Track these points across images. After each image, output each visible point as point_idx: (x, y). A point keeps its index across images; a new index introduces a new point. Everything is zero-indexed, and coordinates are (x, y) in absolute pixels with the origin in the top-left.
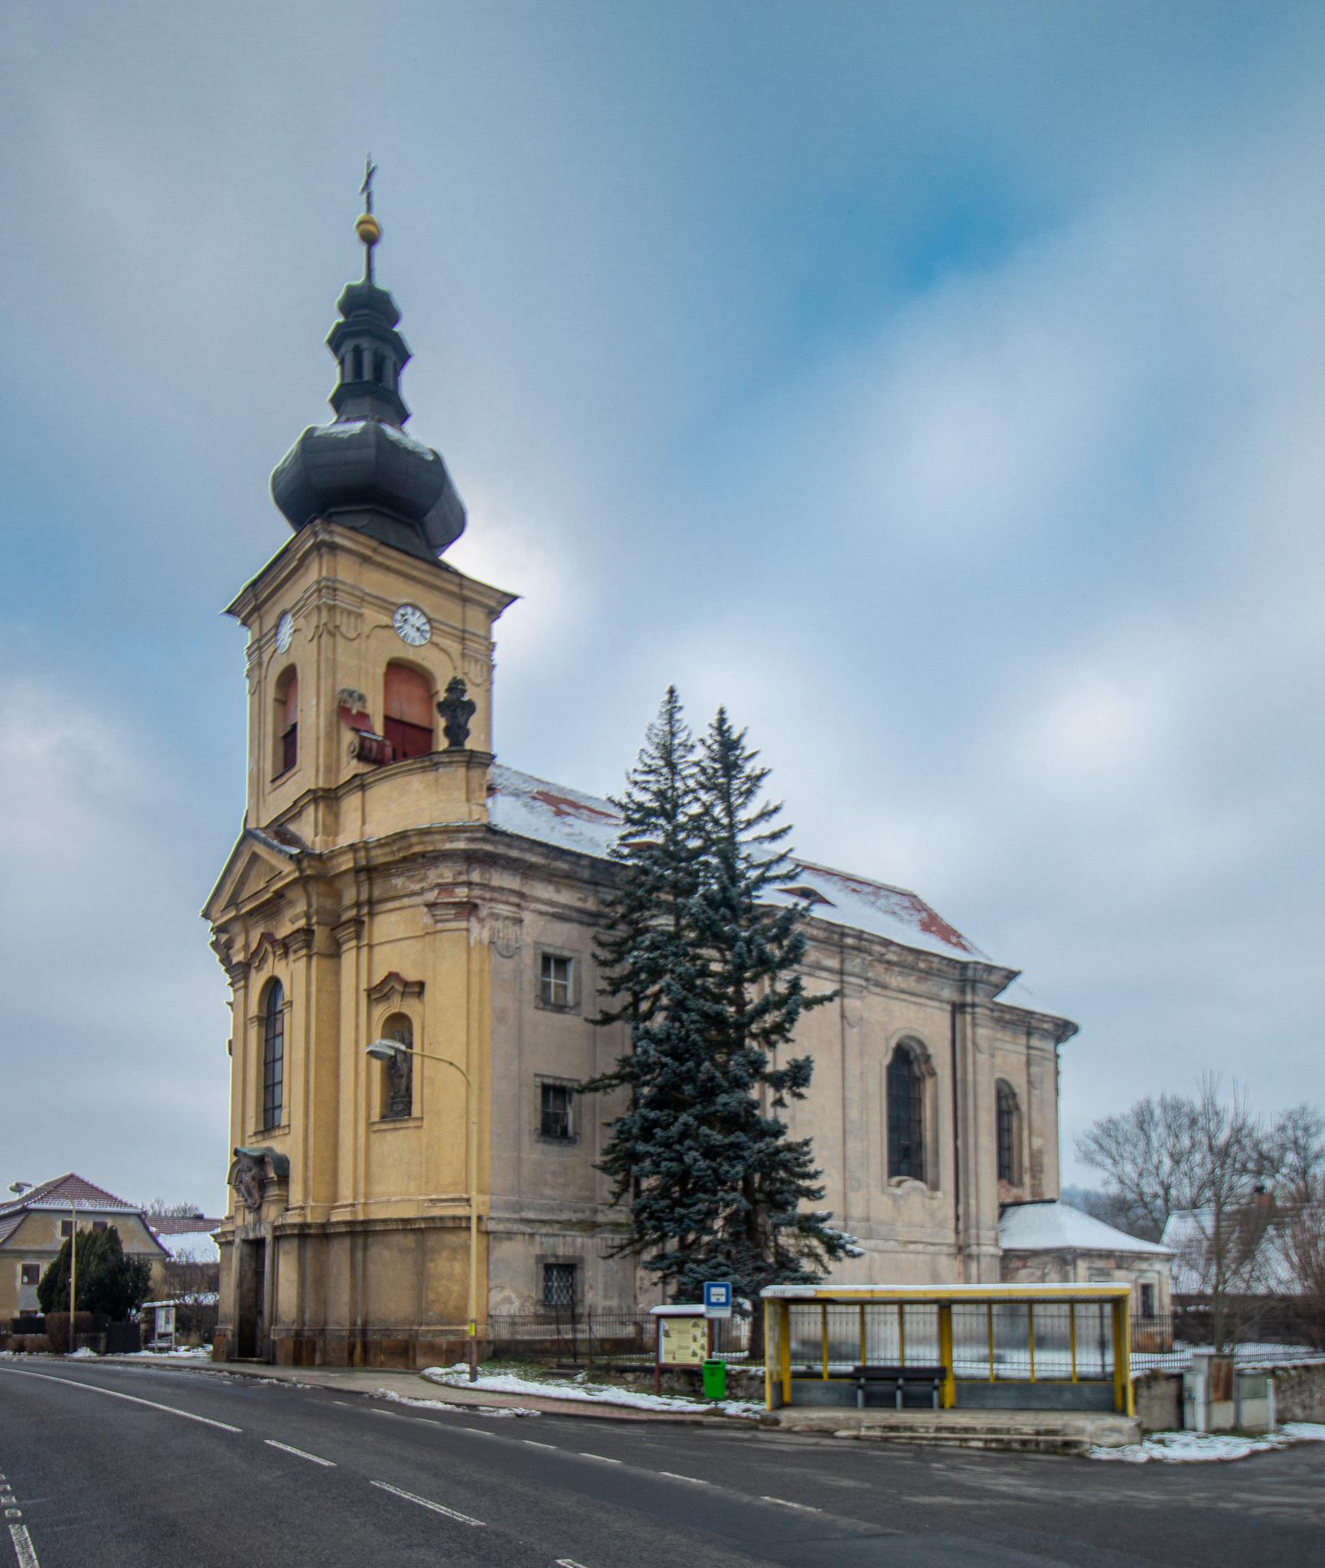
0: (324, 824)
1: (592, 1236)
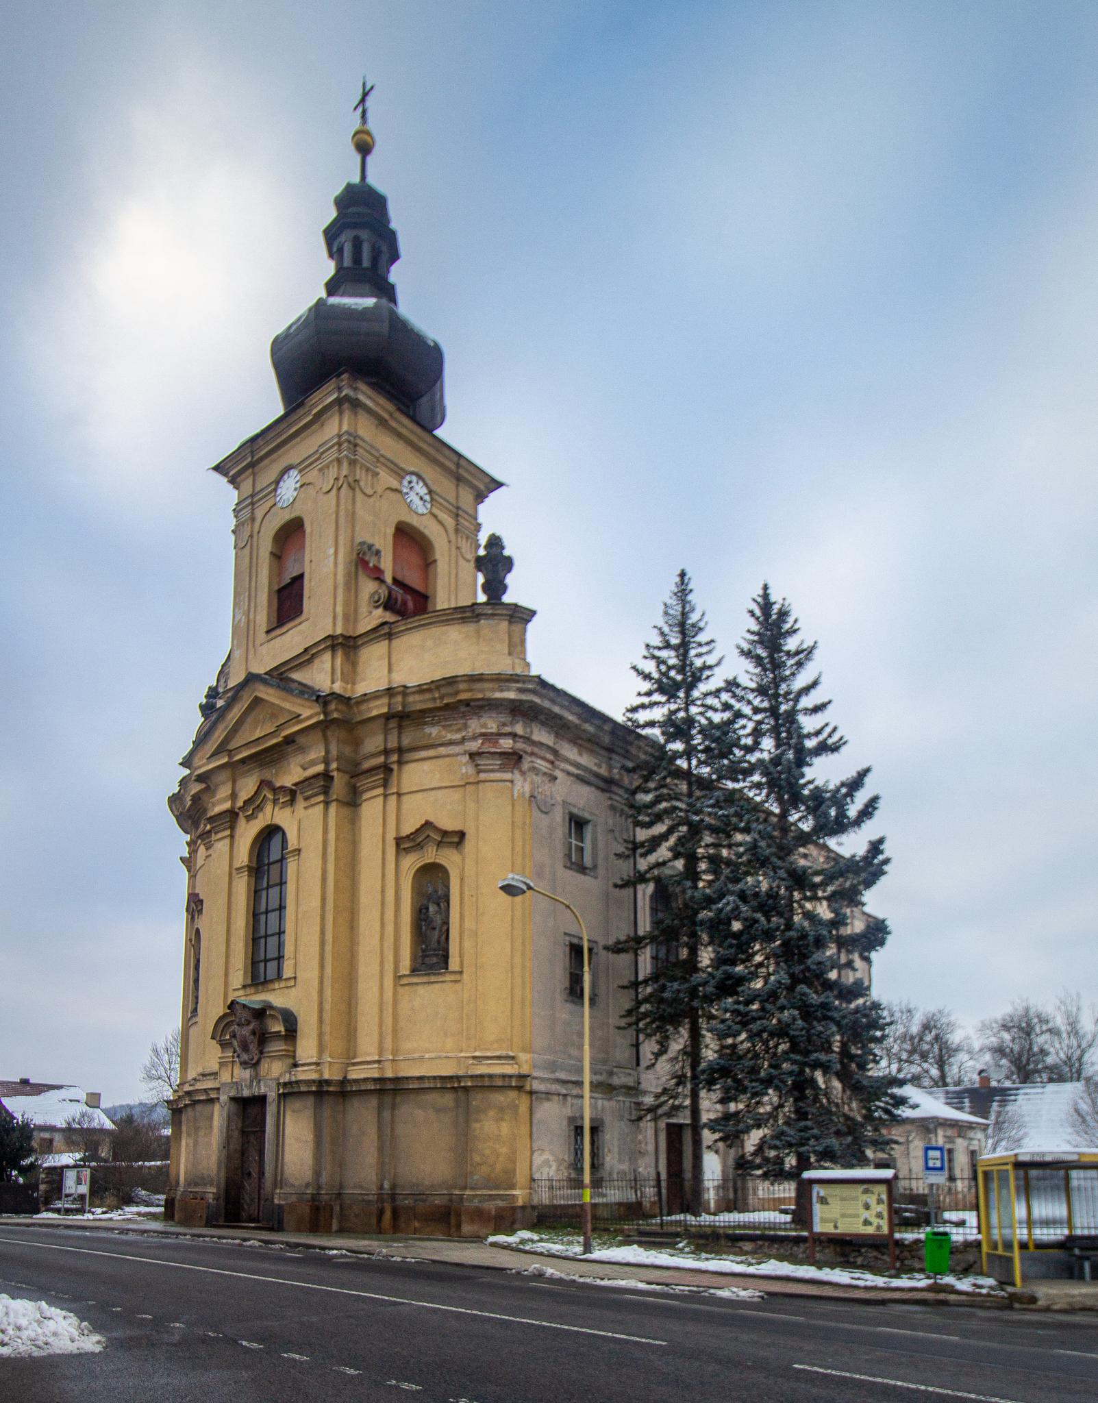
0: (342, 673)
1: (610, 1099)
